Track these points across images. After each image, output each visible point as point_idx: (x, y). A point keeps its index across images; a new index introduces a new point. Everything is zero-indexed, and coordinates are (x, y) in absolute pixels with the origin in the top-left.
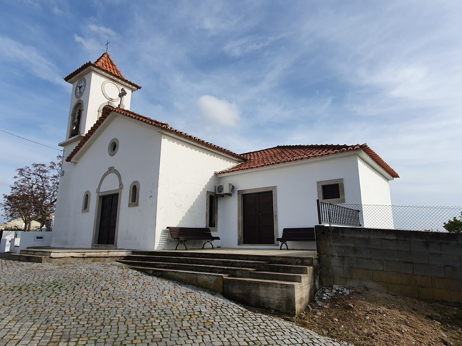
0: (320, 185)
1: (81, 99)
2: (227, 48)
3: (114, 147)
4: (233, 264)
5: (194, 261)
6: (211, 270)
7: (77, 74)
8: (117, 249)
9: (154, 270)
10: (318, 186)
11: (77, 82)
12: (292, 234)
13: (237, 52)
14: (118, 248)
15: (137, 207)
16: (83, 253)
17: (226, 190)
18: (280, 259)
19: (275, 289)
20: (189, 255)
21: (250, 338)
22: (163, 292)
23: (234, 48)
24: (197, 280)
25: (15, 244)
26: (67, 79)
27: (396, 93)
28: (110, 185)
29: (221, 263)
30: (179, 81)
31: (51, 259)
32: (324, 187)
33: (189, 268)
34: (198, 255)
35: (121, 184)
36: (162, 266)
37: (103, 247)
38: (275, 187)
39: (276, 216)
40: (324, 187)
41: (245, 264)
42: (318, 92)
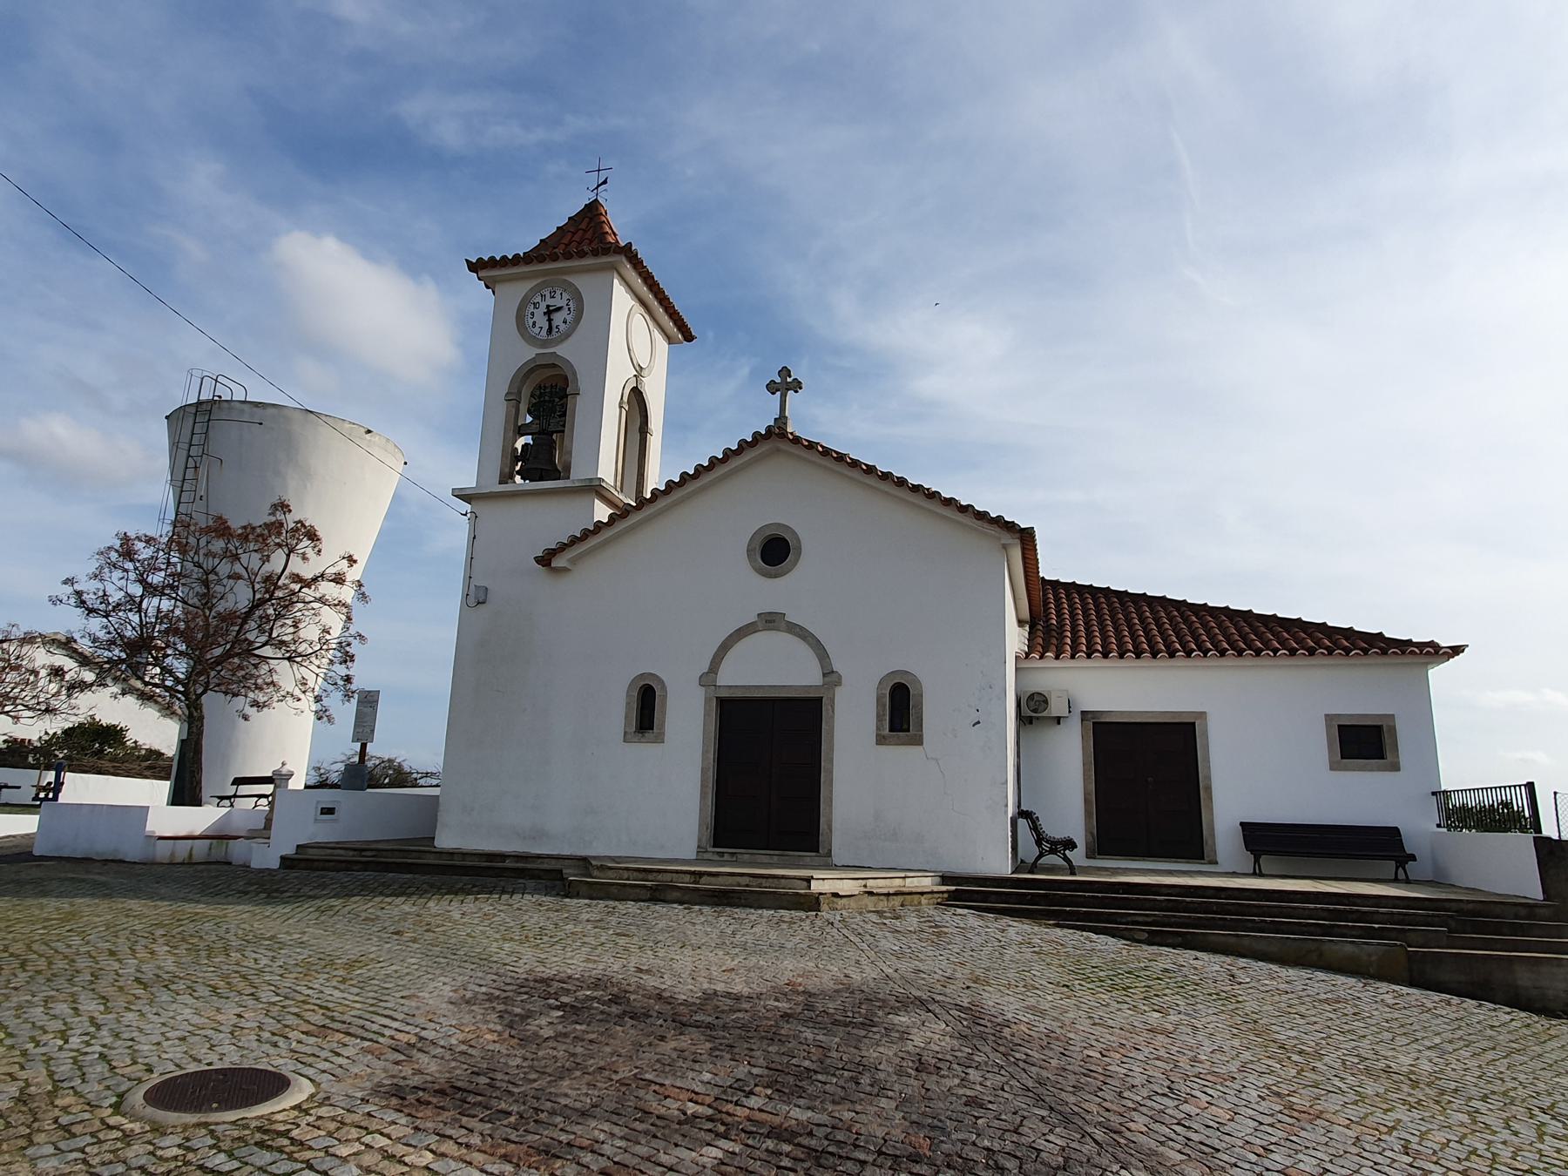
0: (1335, 724)
1: (563, 350)
2: (413, 108)
3: (775, 551)
7: (656, 296)
8: (836, 867)
9: (1149, 932)
10: (1328, 727)
13: (449, 134)
14: (836, 860)
17: (1057, 708)
21: (406, 1159)
23: (441, 118)
25: (149, 828)
26: (474, 267)
27: (929, 385)
29: (1325, 914)
30: (202, 180)
32: (1342, 729)
35: (828, 673)
37: (765, 859)
38: (1202, 715)
39: (1209, 789)
40: (1342, 729)
42: (710, 334)
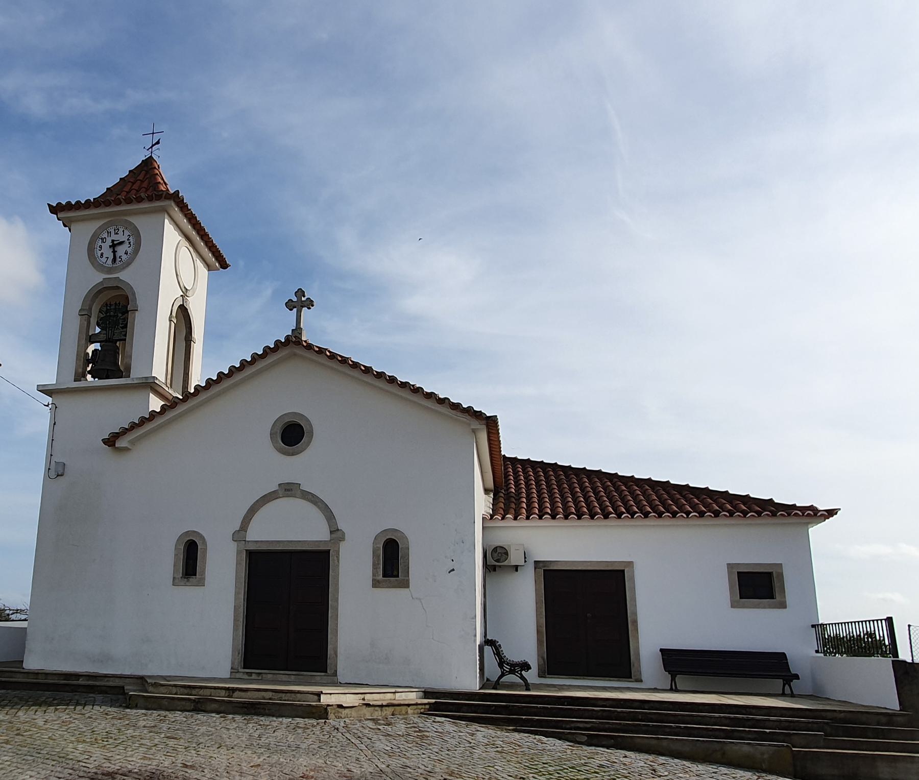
1: (124, 276)
3: (292, 434)
4: (593, 715)
5: (653, 716)
6: (689, 732)
7: (198, 233)
8: (340, 684)
11: (101, 223)
12: (679, 663)
15: (406, 590)
16: (362, 696)
17: (515, 558)
18: (842, 715)
19: (909, 766)
20: (610, 702)
22: (104, 777)
24: (724, 754)
27: (414, 304)
28: (289, 527)
29: (727, 721)
31: (340, 710)
33: (668, 730)
34: (636, 704)
35: (334, 530)
36: (581, 725)
39: (635, 622)
41: (787, 724)
